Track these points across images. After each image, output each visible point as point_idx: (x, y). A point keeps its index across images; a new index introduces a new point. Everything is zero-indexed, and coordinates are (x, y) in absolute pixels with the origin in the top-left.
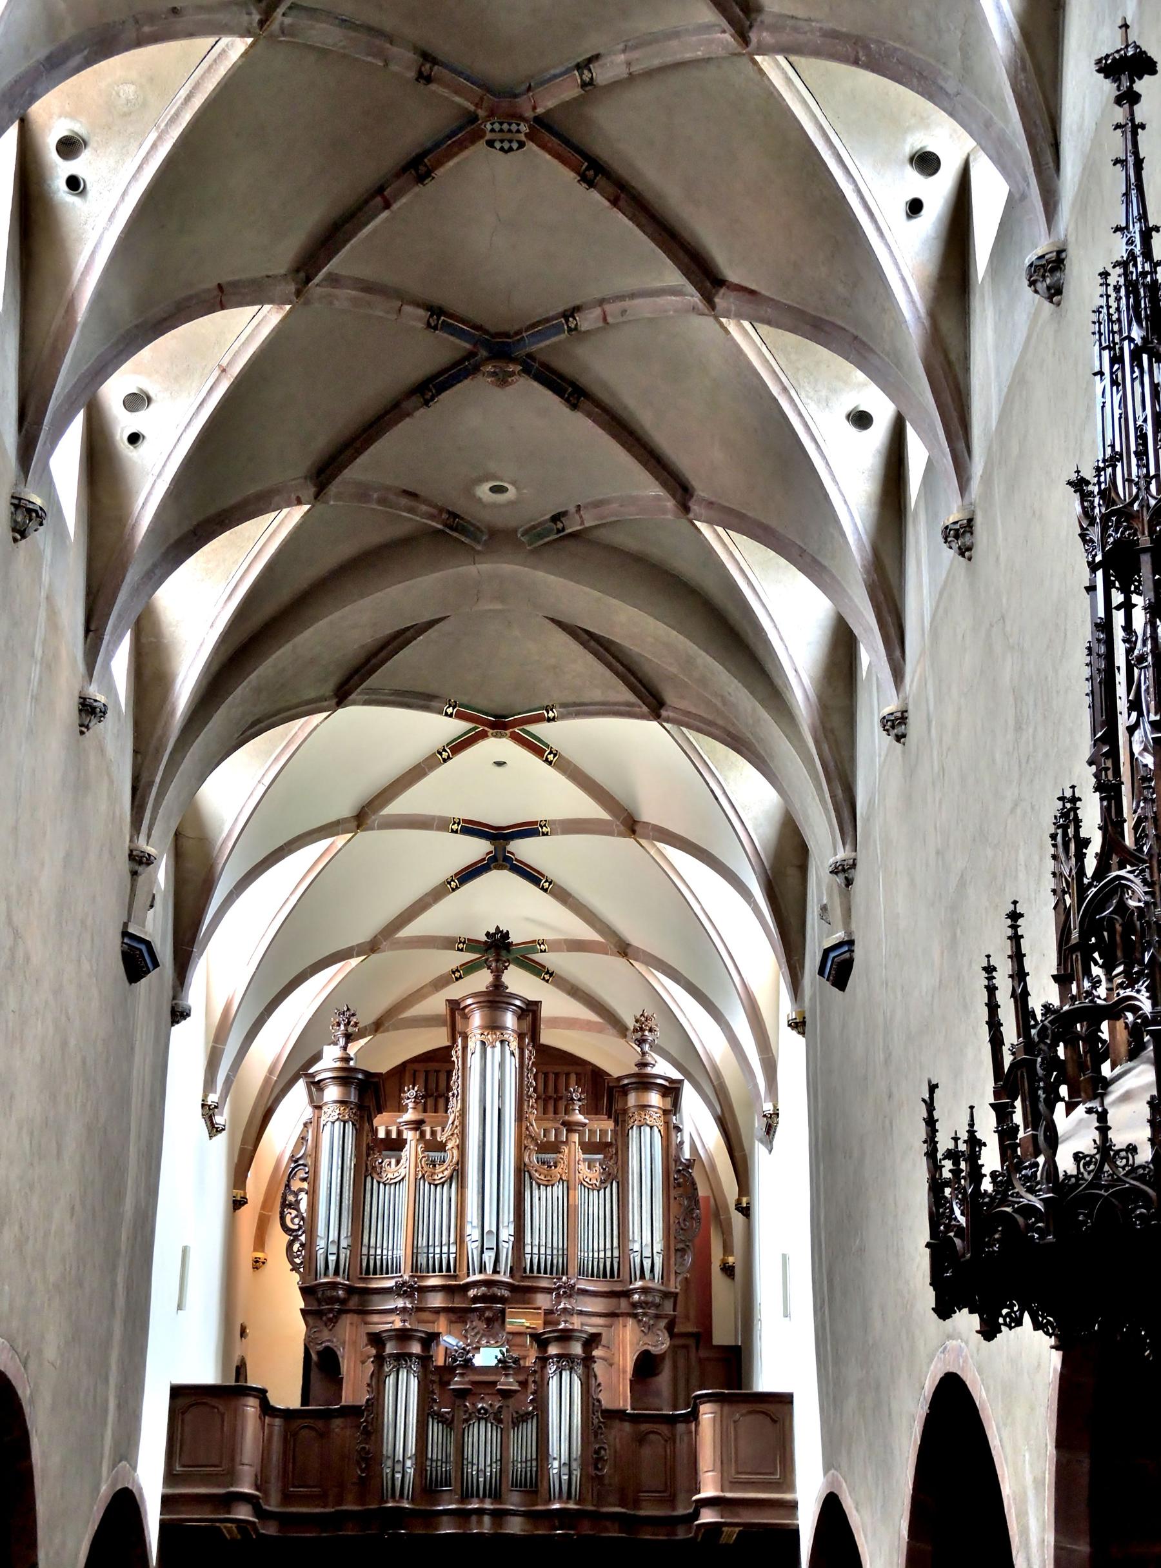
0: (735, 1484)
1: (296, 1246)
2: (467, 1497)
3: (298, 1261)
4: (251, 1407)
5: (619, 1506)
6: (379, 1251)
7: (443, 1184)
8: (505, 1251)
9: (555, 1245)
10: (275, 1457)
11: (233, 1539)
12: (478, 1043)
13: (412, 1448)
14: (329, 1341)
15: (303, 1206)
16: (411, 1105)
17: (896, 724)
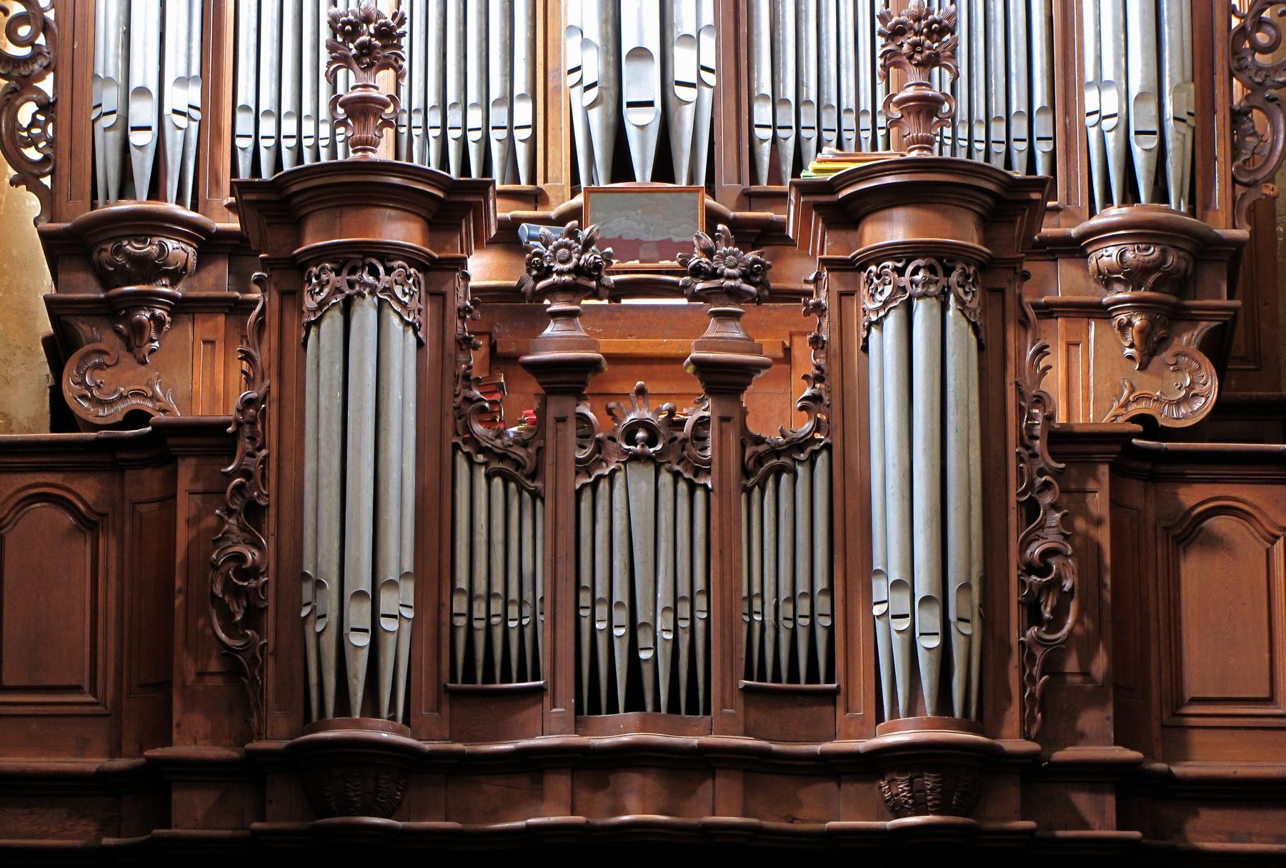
2: (595, 709)
3: (32, 154)
6: (289, 126)
13: (400, 553)
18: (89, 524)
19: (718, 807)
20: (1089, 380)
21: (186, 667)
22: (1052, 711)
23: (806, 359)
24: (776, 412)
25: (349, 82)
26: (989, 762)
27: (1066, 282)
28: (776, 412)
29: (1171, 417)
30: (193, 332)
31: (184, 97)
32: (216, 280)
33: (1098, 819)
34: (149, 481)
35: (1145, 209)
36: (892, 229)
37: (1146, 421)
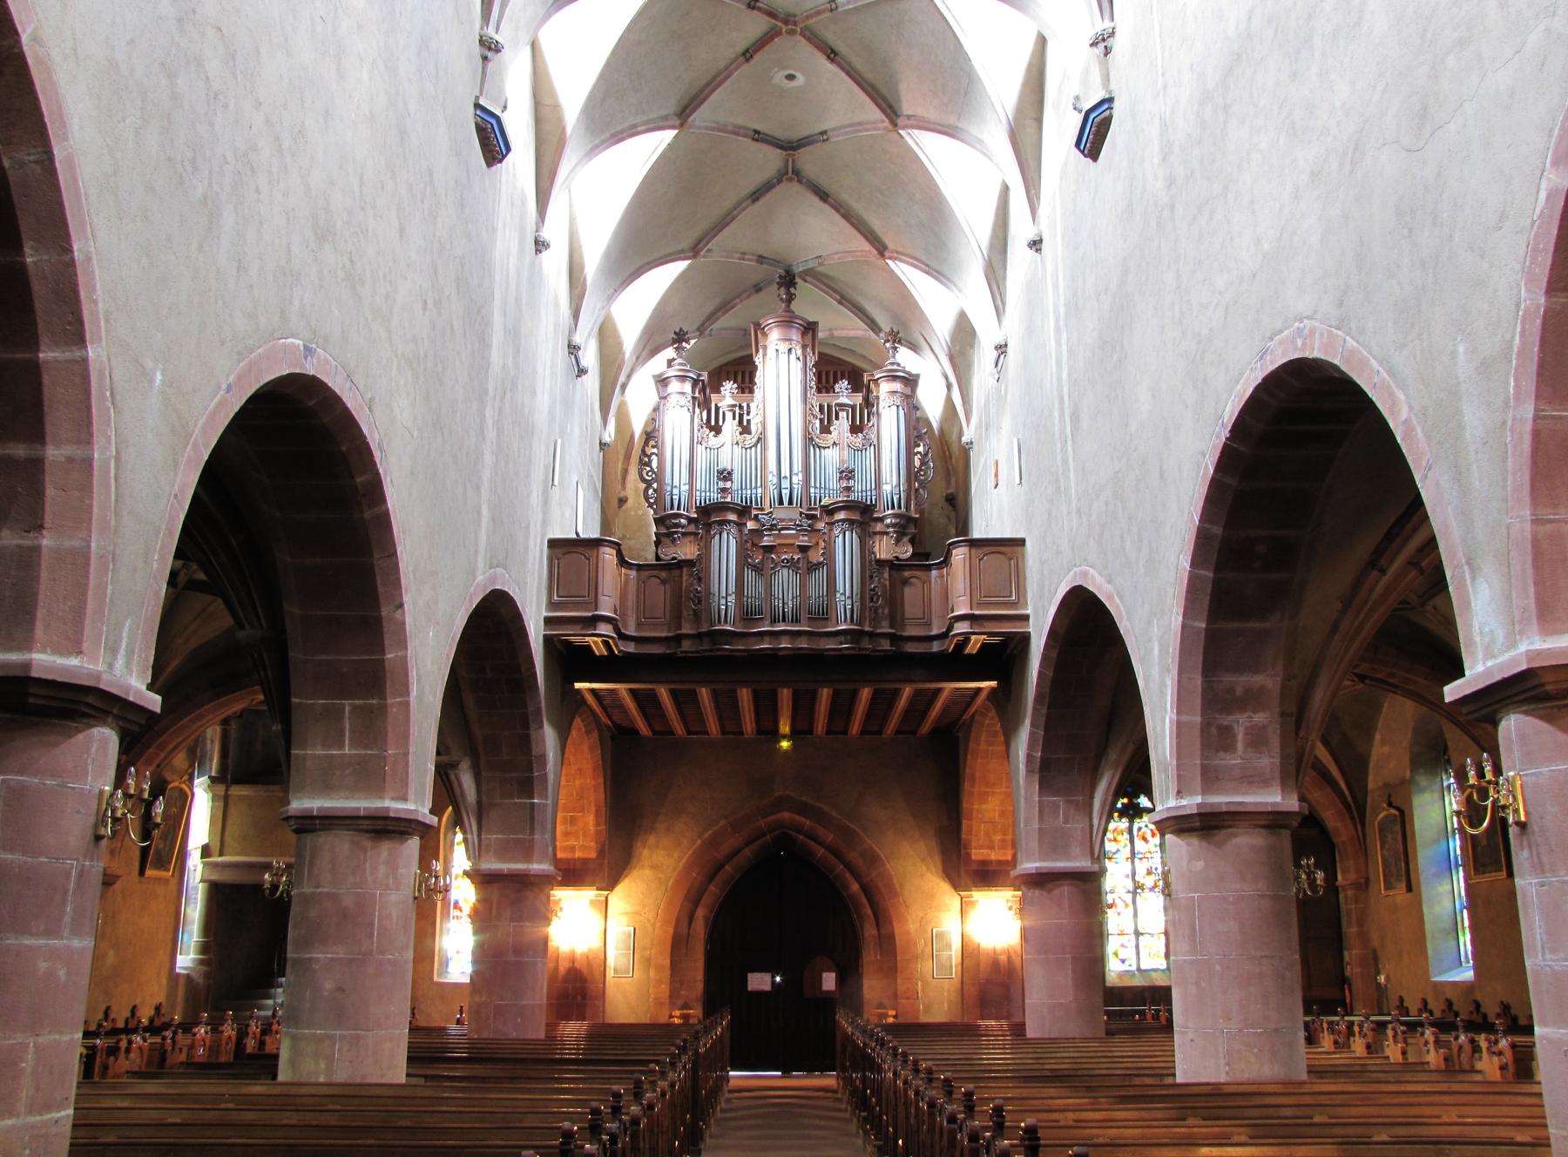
0: (981, 605)
4: (609, 555)
10: (632, 596)
11: (602, 657)
13: (732, 588)
15: (654, 464)
17: (1036, 244)
18: (664, 582)
19: (803, 644)
20: (884, 548)
21: (685, 613)
22: (875, 621)
23: (822, 544)
24: (816, 556)
25: (721, 484)
26: (861, 633)
27: (879, 527)
28: (816, 556)
29: (902, 556)
30: (687, 540)
31: (685, 488)
32: (692, 528)
33: (886, 645)
34: (677, 572)
35: (896, 511)
36: (841, 515)
37: (897, 558)
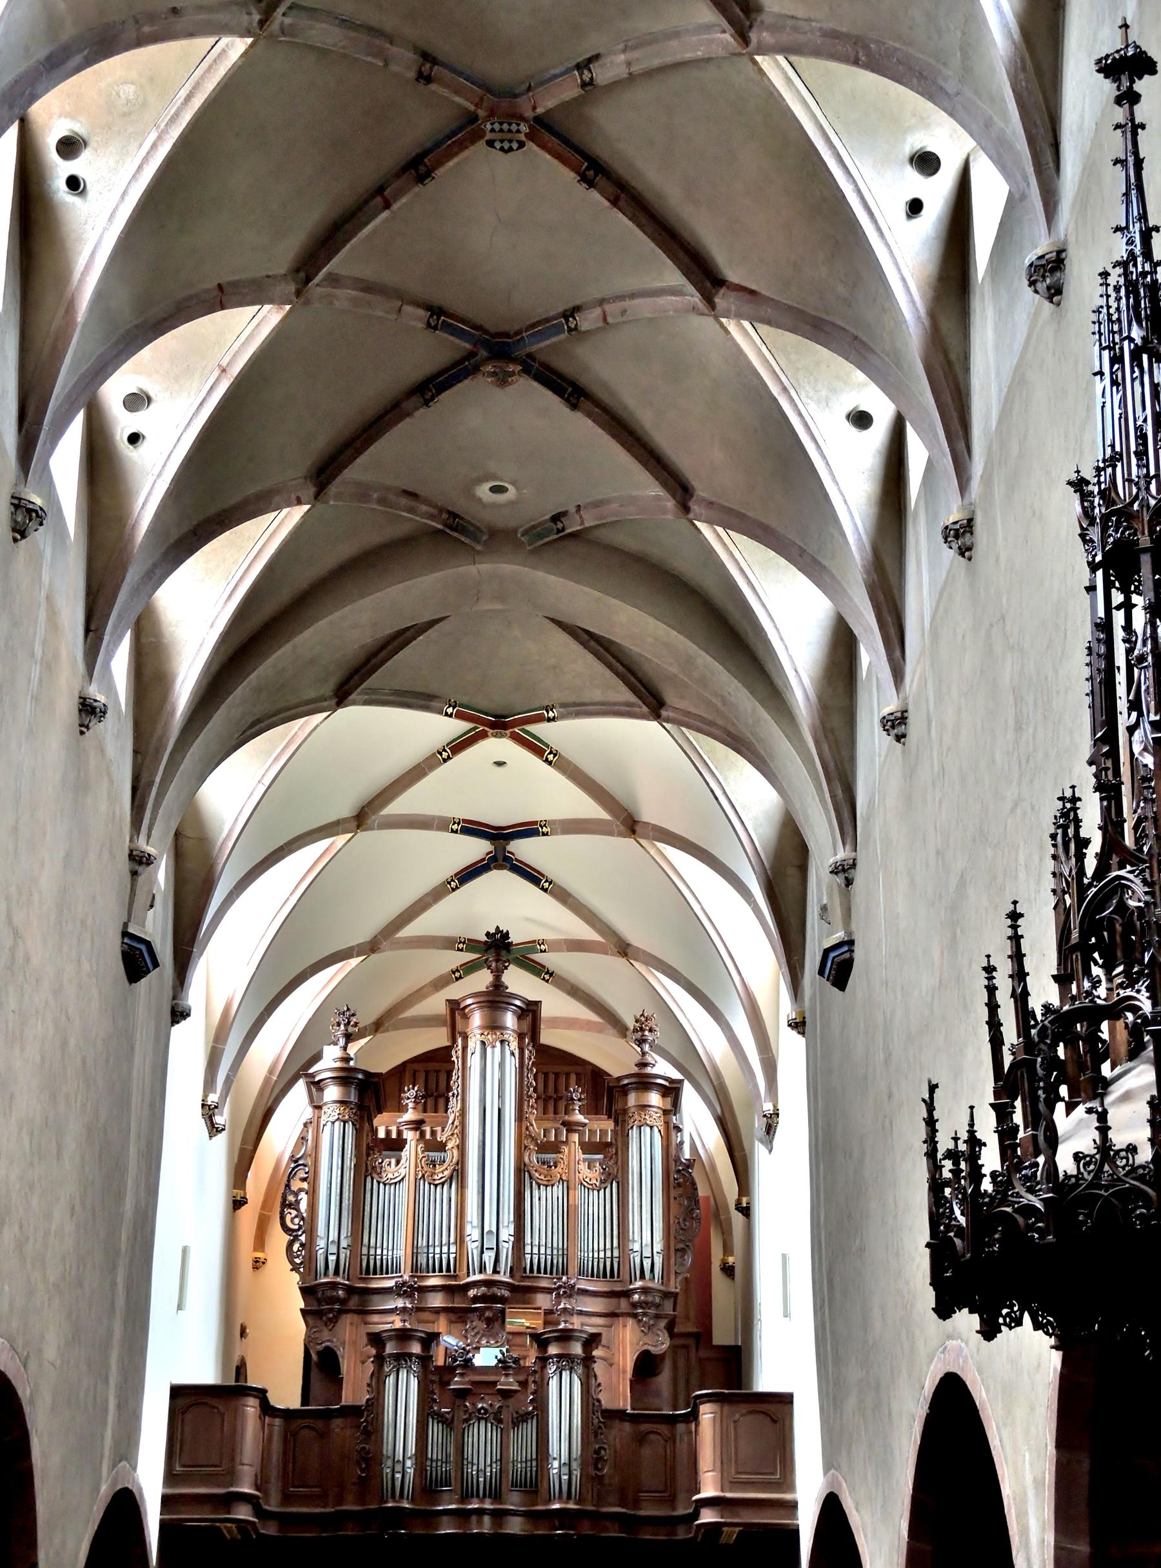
0: (735, 1484)
1: (296, 1246)
2: (467, 1497)
3: (298, 1261)
4: (251, 1407)
5: (619, 1506)
6: (379, 1251)
7: (443, 1184)
8: (505, 1251)
9: (555, 1245)
10: (275, 1457)
11: (233, 1539)
12: (478, 1043)
13: (412, 1448)
14: (329, 1341)
15: (303, 1206)
16: (411, 1105)
17: (896, 724)
